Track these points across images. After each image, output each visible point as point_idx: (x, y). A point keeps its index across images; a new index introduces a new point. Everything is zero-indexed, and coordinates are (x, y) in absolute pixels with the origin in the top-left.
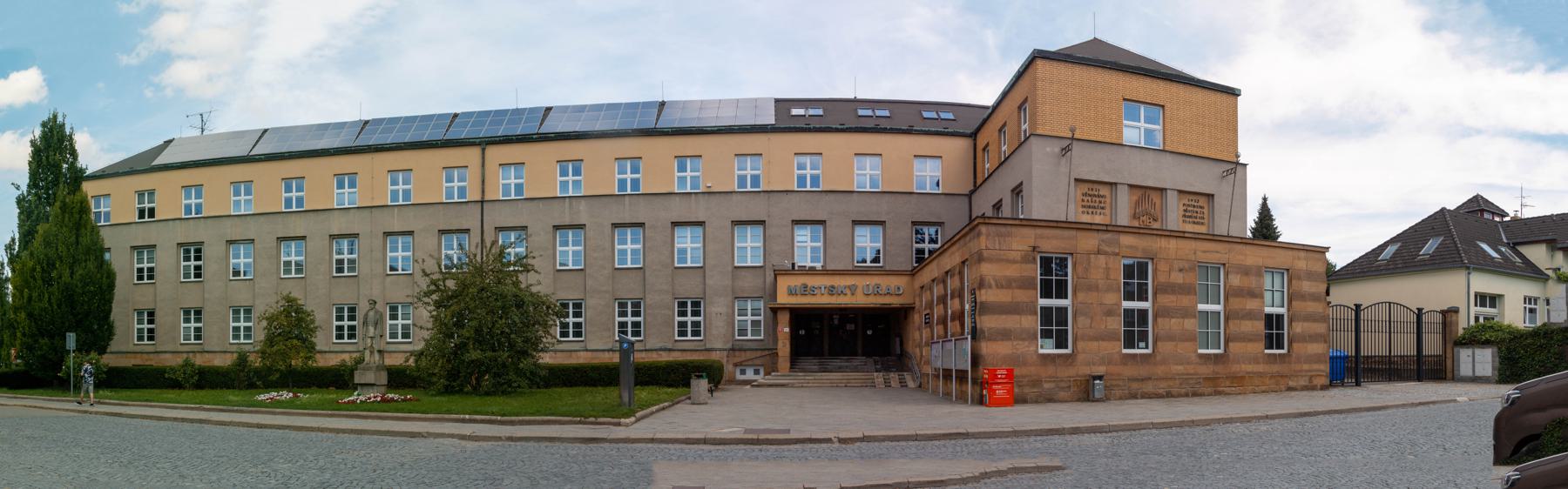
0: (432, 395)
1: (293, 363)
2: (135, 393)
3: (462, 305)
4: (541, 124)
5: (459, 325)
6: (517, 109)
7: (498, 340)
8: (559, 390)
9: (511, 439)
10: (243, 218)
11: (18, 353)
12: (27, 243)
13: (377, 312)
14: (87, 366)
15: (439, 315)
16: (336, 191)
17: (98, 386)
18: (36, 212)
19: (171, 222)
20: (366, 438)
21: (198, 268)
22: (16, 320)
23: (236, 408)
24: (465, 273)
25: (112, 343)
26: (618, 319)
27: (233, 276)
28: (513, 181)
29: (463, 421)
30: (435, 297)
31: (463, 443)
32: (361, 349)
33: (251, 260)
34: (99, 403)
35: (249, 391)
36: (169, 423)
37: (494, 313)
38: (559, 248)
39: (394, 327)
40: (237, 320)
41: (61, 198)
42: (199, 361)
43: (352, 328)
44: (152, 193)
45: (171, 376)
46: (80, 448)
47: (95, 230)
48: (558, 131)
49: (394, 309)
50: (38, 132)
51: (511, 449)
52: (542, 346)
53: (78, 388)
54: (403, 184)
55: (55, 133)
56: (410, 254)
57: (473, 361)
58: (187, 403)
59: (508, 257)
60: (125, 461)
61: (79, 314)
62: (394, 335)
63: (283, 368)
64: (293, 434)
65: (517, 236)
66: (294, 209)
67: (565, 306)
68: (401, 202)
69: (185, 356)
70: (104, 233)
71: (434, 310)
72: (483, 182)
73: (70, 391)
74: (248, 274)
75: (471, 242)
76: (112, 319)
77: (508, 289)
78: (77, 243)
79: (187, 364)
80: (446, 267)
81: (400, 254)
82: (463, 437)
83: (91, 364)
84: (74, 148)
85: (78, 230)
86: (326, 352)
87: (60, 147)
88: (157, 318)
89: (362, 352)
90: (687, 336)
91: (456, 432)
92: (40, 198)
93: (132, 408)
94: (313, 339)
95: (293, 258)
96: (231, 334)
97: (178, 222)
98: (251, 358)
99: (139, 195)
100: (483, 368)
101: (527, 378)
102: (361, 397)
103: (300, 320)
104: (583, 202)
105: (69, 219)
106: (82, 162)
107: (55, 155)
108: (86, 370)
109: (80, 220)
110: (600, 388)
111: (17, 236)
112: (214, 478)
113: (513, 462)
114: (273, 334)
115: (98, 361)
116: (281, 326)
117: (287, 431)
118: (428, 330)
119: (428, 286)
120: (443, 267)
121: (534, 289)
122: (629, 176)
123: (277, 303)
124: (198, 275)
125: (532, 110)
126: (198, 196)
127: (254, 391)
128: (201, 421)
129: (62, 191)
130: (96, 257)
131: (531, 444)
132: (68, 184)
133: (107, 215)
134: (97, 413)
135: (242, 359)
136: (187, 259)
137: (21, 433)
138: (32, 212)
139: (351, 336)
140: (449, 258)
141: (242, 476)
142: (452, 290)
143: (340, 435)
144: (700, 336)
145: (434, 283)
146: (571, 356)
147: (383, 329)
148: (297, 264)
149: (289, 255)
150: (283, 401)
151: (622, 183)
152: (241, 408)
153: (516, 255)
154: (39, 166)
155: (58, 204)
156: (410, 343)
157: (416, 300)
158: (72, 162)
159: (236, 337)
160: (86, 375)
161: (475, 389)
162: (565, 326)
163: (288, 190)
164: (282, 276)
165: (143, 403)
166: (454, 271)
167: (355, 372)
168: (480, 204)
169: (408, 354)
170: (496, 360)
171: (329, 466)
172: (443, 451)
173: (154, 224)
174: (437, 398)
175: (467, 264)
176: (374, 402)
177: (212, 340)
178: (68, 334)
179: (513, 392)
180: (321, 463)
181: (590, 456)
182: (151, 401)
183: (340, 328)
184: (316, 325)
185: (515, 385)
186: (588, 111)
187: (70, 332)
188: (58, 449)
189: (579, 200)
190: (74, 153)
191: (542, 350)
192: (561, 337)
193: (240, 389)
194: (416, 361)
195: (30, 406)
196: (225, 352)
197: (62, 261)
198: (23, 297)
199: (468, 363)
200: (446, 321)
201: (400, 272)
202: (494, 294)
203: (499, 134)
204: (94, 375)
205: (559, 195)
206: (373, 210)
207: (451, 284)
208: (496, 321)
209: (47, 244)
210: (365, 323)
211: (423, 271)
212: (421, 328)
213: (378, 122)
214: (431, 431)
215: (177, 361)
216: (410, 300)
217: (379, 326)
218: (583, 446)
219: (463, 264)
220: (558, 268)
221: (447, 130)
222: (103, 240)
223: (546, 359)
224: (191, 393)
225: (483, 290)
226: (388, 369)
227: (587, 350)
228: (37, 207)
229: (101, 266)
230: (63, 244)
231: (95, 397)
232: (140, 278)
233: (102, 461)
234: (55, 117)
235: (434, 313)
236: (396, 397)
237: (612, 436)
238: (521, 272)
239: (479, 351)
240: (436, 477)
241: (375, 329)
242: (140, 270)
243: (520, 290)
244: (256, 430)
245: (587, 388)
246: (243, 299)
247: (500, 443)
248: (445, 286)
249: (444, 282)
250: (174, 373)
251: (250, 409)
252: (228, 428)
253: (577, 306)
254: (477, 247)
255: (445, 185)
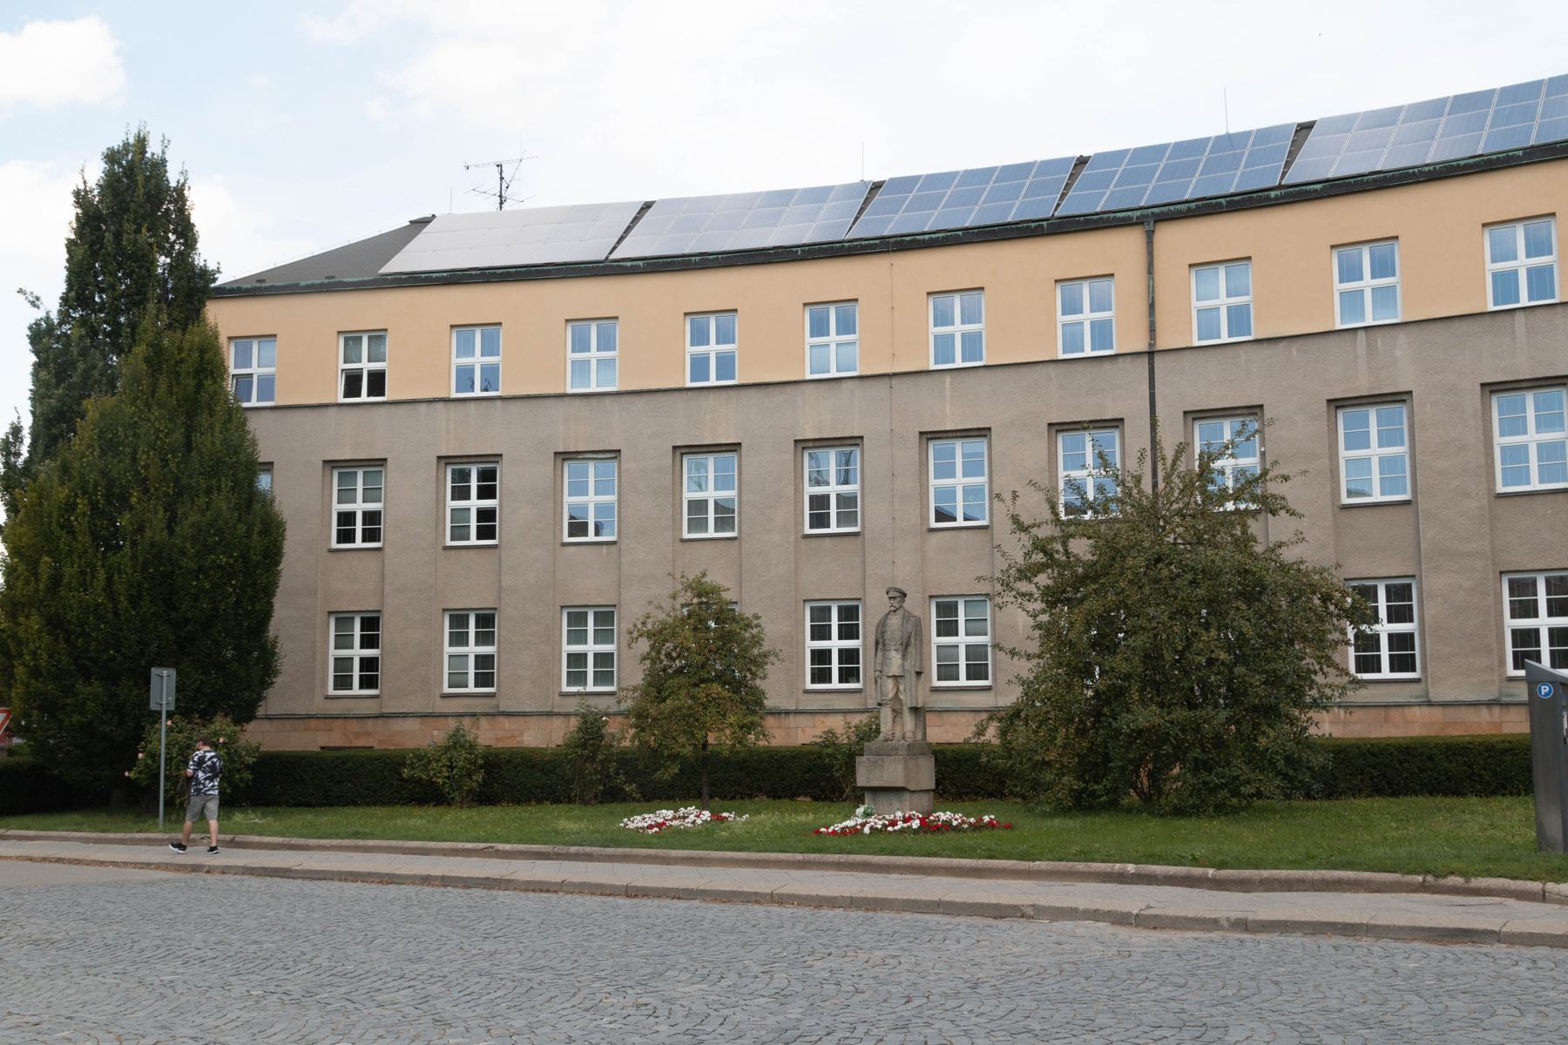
0: (1044, 815)
1: (711, 739)
2: (326, 818)
3: (1111, 597)
4: (1288, 164)
5: (1104, 644)
6: (1229, 137)
7: (1203, 682)
8: (1362, 803)
9: (1242, 925)
10: (594, 401)
11: (15, 721)
12: (54, 440)
13: (907, 616)
14: (205, 752)
15: (1054, 622)
16: (809, 340)
17: (231, 801)
18: (81, 366)
19: (423, 408)
20: (885, 918)
21: (486, 515)
22: (14, 636)
23: (573, 849)
24: (1116, 520)
25: (270, 693)
26: (1512, 623)
27: (571, 535)
28: (1223, 301)
29: (1122, 878)
30: (1043, 579)
31: (1124, 933)
32: (871, 704)
33: (613, 498)
34: (233, 844)
35: (606, 808)
36: (409, 890)
37: (1189, 616)
38: (1344, 454)
39: (947, 652)
40: (578, 637)
41: (150, 336)
42: (487, 735)
43: (849, 656)
44: (378, 337)
45: (417, 774)
46: (179, 962)
47: (235, 418)
48: (1330, 175)
49: (947, 609)
50: (95, 173)
51: (1244, 952)
52: (1314, 692)
53: (177, 806)
54: (963, 323)
55: (140, 178)
56: (982, 480)
57: (1140, 732)
58: (456, 840)
59: (1219, 479)
60: (297, 992)
61: (187, 621)
62: (948, 672)
63: (687, 750)
64: (713, 910)
65: (1238, 427)
66: (713, 382)
67: (1369, 593)
68: (959, 364)
69: (452, 724)
70: (256, 425)
71: (1044, 611)
72: (1152, 307)
73: (158, 816)
74: (604, 531)
75: (1129, 449)
76: (271, 633)
77: (1223, 556)
78: (189, 447)
79: (457, 742)
80: (1069, 508)
81: (959, 481)
82: (1120, 919)
83: (215, 746)
84: (188, 218)
85: (191, 415)
86: (787, 713)
87: (153, 214)
88: (385, 633)
89: (874, 712)
90: (830, 681)
91: (1106, 905)
92: (94, 332)
93: (318, 855)
94: (758, 682)
95: (711, 494)
96: (565, 669)
97: (440, 406)
98: (613, 728)
99: (346, 340)
100: (1167, 749)
101: (1279, 773)
102: (872, 820)
103: (726, 637)
104: (1402, 337)
105: (170, 386)
106: (207, 254)
107: (138, 231)
108: (202, 760)
109: (197, 392)
110: (1473, 800)
111: (27, 422)
112: (519, 1023)
113: (1254, 984)
114: (664, 670)
115: (232, 739)
116: (683, 650)
117: (696, 903)
118: (1029, 657)
119: (1027, 555)
120: (1061, 509)
121: (1289, 555)
122: (1522, 263)
123: (674, 597)
124: (486, 532)
125: (1264, 135)
126: (490, 348)
127: (617, 807)
128: (489, 883)
129: (154, 319)
130: (237, 483)
131: (1296, 939)
132: (169, 304)
133: (267, 384)
134: (225, 870)
135: (591, 730)
136: (461, 493)
137: (18, 931)
138: (73, 364)
139: (846, 675)
140: (1075, 487)
141: (588, 1015)
142: (1084, 564)
143: (823, 912)
144: (1413, 670)
145: (1040, 546)
146: (1387, 720)
147: (923, 656)
148: (719, 507)
149: (700, 486)
150: (686, 830)
151: (1505, 284)
152: (588, 849)
153: (1240, 473)
154: (94, 255)
155: (140, 350)
156: (988, 689)
157: (999, 588)
158: (180, 253)
159: (577, 677)
160: (201, 775)
161: (1147, 798)
162: (1368, 643)
163: (700, 337)
164: (686, 536)
165: (346, 842)
166: (1087, 517)
167: (858, 759)
168: (1146, 359)
169: (984, 716)
170: (1197, 730)
171: (797, 986)
172: (1075, 952)
173: (384, 410)
174: (1056, 822)
175: (1120, 501)
176: (902, 831)
177: (515, 690)
178: (155, 671)
179: (1243, 809)
180: (780, 980)
181: (1454, 977)
182: (365, 836)
183: (821, 656)
184: (765, 648)
185: (1247, 790)
186: (1403, 122)
187: (162, 665)
188: (119, 967)
189: (1393, 332)
190: (187, 232)
191: (1316, 705)
192: (1358, 671)
193: (586, 803)
194: (1003, 733)
195: (44, 860)
196: (549, 714)
197: (146, 491)
198: (36, 574)
199: (1130, 736)
200: (1072, 636)
201: (960, 522)
202: (1185, 568)
203: (1187, 197)
204: (225, 775)
205: (1339, 326)
206: (894, 381)
207: (1081, 548)
208: (1194, 634)
209: (108, 445)
210: (880, 643)
211: (1015, 519)
212: (1013, 653)
213: (904, 184)
214: (1043, 901)
215: (435, 736)
216: (984, 588)
217: (911, 649)
218: (1436, 950)
219: (1108, 500)
220: (1345, 500)
221: (1063, 196)
222: (254, 443)
223: (1326, 726)
224: (464, 814)
225: (1159, 560)
226: (935, 753)
227: (1430, 704)
228: (84, 353)
229: (249, 506)
230: (152, 447)
231: (220, 831)
232: (346, 536)
233: (236, 992)
234: (141, 142)
235: (1044, 618)
236: (956, 819)
237: (1515, 927)
238: (1254, 514)
239: (1154, 707)
240: (1058, 1017)
241: (904, 656)
242: (347, 518)
243: (1254, 556)
244: (621, 901)
245: (1439, 799)
246: (592, 588)
247: (1215, 935)
248: (1067, 553)
249: (1065, 544)
250: (425, 768)
251: (610, 850)
252: (554, 897)
253: (1399, 593)
254: (1141, 459)
255: (1062, 319)
